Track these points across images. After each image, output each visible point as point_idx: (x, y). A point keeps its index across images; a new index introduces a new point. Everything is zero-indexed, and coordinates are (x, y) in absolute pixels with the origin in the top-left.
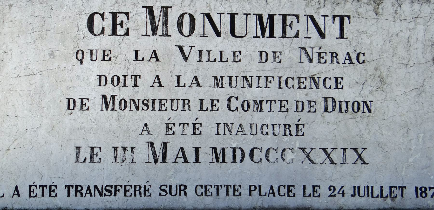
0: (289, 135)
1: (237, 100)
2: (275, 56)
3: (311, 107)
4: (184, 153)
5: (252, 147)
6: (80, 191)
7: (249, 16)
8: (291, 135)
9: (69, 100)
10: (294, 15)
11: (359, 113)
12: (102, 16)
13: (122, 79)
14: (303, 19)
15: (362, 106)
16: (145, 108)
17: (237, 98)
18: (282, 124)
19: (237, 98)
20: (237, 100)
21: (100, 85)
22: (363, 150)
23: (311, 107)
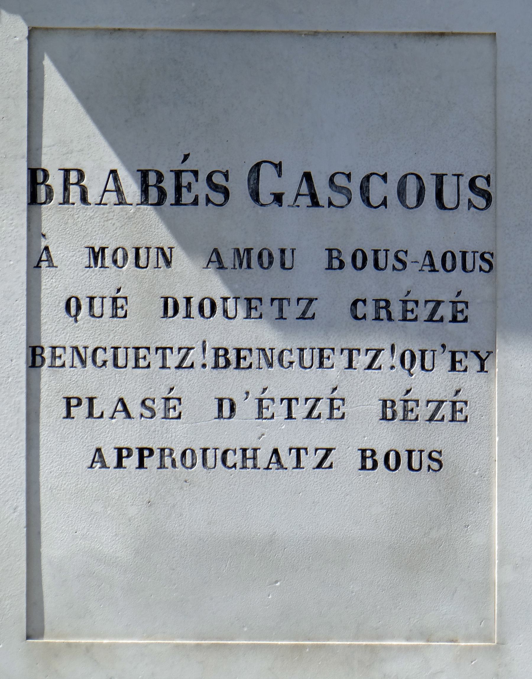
0: (386, 321)
1: (386, 182)
2: (250, 306)
3: (407, 311)
4: (101, 456)
5: (143, 398)
6: (337, 258)
7: (266, 467)
8: (390, 318)
9: (220, 401)
10: (268, 399)
11: (114, 247)
12: (235, 451)
13: (277, 256)
14: (255, 353)
15: (275, 358)
16: (339, 199)
17: (384, 177)
18: (173, 369)
19: (384, 177)
20: (386, 182)
21: (220, 416)
22: (430, 470)
23: (407, 311)
